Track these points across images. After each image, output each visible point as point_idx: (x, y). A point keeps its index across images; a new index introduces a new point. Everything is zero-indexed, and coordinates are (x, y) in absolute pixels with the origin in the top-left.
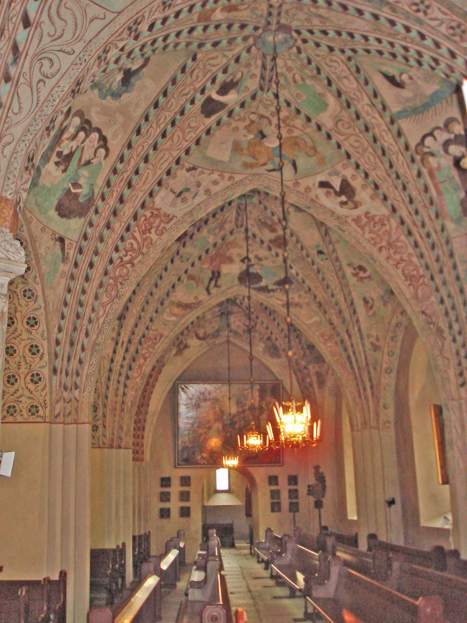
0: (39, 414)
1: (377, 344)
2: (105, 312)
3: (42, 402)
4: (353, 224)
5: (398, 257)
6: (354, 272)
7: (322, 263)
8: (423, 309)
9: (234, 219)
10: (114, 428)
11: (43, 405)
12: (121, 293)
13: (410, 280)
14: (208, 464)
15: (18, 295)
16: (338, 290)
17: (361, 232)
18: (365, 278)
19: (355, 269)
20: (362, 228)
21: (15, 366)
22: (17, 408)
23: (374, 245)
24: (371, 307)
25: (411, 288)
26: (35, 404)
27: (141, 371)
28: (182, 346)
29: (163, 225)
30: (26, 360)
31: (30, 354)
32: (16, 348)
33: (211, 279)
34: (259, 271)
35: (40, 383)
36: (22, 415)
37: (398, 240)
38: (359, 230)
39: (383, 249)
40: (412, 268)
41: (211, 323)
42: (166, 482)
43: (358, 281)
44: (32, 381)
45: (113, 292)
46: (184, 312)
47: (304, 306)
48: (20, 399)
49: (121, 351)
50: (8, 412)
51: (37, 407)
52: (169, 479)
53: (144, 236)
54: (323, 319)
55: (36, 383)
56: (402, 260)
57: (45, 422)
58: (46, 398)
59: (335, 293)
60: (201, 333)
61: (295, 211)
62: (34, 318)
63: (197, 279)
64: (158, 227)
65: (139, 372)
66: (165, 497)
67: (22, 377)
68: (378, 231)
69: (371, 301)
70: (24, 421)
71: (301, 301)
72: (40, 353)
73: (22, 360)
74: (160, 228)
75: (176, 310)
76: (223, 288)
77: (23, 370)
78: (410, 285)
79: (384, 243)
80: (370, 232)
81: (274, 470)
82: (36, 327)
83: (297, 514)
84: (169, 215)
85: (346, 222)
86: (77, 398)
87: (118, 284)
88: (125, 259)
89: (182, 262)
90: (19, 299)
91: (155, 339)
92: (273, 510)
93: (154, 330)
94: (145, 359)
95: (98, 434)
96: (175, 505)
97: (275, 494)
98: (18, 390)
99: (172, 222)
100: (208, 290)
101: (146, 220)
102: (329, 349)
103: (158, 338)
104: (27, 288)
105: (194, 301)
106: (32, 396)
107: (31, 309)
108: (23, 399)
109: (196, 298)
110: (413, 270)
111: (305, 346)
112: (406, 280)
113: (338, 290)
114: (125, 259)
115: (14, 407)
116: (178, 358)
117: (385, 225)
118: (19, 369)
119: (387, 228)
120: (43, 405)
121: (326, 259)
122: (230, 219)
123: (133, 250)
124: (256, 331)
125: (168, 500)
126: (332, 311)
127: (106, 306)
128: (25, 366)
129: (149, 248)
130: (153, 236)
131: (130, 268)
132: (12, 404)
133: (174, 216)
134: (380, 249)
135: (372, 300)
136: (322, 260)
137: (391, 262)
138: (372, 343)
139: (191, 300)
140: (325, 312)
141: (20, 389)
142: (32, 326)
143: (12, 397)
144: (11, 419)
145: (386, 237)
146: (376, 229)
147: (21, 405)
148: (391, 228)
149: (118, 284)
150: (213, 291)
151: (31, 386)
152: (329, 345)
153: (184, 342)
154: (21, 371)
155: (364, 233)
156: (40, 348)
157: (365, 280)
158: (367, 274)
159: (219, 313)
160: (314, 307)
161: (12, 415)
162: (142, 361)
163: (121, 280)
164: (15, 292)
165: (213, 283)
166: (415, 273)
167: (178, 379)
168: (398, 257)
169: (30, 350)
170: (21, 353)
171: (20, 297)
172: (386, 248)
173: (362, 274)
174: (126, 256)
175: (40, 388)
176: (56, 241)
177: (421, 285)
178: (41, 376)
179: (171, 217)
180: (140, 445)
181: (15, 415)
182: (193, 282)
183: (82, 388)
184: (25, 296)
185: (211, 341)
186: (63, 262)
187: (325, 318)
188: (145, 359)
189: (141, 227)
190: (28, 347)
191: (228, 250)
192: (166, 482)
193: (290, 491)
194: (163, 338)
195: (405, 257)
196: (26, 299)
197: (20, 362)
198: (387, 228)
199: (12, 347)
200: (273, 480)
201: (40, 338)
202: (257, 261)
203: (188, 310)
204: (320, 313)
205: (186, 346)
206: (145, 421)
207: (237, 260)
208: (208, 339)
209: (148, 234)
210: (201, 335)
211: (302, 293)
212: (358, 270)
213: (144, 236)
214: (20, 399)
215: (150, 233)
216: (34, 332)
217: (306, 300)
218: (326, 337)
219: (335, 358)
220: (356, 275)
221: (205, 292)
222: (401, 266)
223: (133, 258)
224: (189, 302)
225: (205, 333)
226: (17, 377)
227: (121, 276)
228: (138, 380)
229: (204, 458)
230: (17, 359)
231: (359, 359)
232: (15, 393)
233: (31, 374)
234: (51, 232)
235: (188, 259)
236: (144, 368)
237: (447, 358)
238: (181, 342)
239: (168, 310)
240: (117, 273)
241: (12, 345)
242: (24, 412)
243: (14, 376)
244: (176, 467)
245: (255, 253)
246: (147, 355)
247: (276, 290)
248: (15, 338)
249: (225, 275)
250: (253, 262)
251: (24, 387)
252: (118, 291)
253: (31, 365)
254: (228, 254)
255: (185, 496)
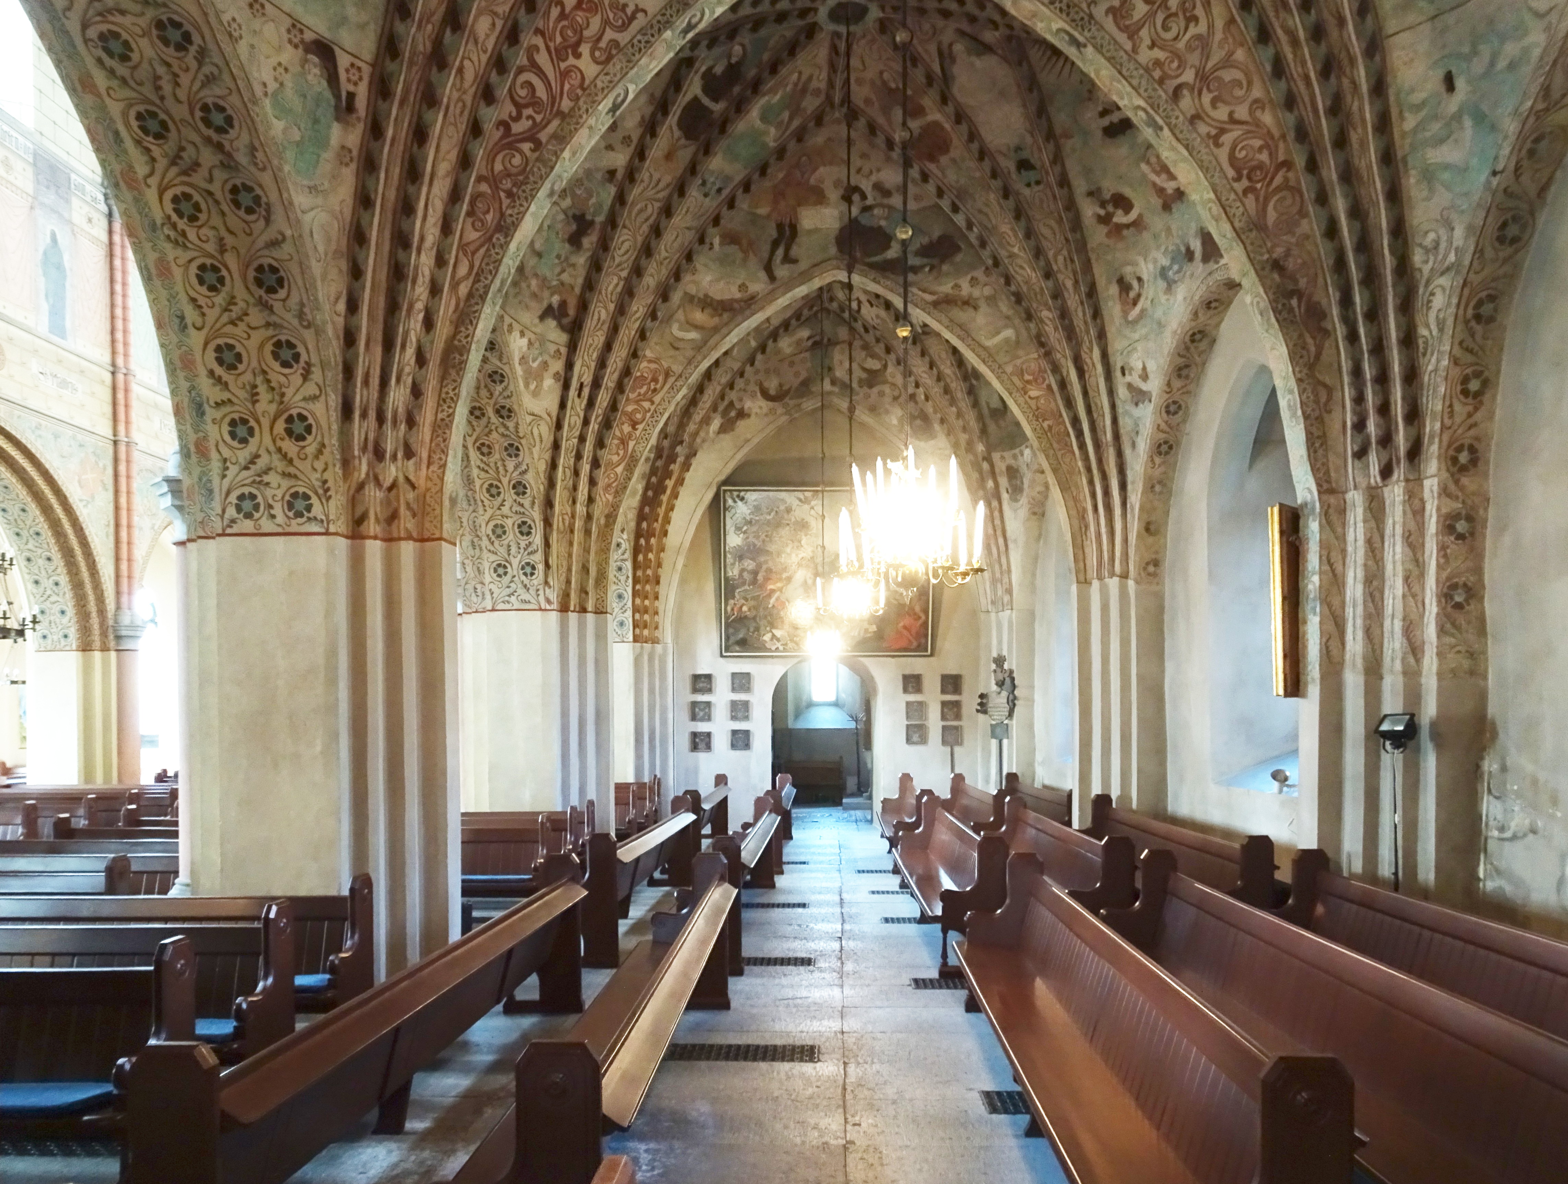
0: (311, 515)
1: (1144, 387)
2: (471, 267)
3: (317, 484)
4: (1109, 23)
5: (1221, 113)
6: (1102, 212)
7: (1027, 192)
8: (1275, 256)
9: (823, 85)
10: (569, 570)
11: (321, 491)
12: (509, 220)
13: (1249, 178)
14: (785, 650)
15: (217, 202)
16: (1060, 258)
17: (1128, 46)
18: (1128, 226)
19: (1103, 205)
20: (1132, 33)
21: (242, 394)
22: (260, 499)
23: (1161, 82)
24: (1135, 303)
25: (1250, 201)
26: (301, 490)
27: (626, 451)
28: (733, 414)
29: (609, 34)
30: (268, 381)
31: (276, 366)
32: (239, 348)
33: (775, 244)
34: (883, 223)
35: (310, 439)
36: (273, 517)
37: (1227, 63)
38: (1122, 38)
39: (1185, 92)
40: (1257, 143)
41: (792, 364)
42: (702, 682)
43: (1109, 235)
44: (289, 432)
45: (489, 217)
46: (716, 320)
47: (983, 305)
48: (266, 479)
49: (577, 406)
50: (239, 509)
51: (306, 497)
52: (709, 677)
53: (563, 65)
54: (1024, 333)
55: (300, 438)
56: (1233, 120)
57: (327, 533)
58: (326, 476)
59: (1055, 268)
60: (772, 385)
61: (969, 52)
62: (274, 270)
63: (744, 242)
64: (599, 39)
65: (621, 452)
66: (699, 712)
67: (265, 422)
68: (1176, 38)
69: (1135, 284)
70: (280, 530)
71: (976, 293)
72: (302, 364)
73: (259, 380)
74: (603, 44)
75: (699, 316)
76: (803, 265)
77: (266, 406)
78: (1245, 192)
79: (1188, 76)
80: (1153, 45)
81: (916, 665)
82: (282, 294)
83: (957, 749)
84: (625, 5)
85: (1091, 16)
86: (412, 477)
87: (502, 195)
88: (518, 128)
89: (706, 195)
90: (223, 214)
91: (655, 380)
92: (909, 741)
93: (650, 361)
94: (634, 425)
95: (535, 582)
96: (720, 727)
97: (915, 710)
98: (257, 456)
99: (635, 26)
100: (768, 269)
101: (563, 16)
102: (1033, 403)
103: (661, 379)
104: (238, 182)
105: (738, 295)
106: (292, 470)
107: (260, 243)
108: (272, 478)
109: (742, 287)
110: (1260, 149)
111: (986, 411)
112: (1238, 179)
113: (1060, 258)
114: (518, 128)
115: (253, 497)
116: (727, 438)
117: (1196, 19)
118: (254, 402)
119: (1202, 28)
120: (321, 491)
121: (1038, 183)
122: (815, 84)
123: (534, 102)
124: (885, 382)
125: (708, 718)
126: (1045, 314)
127: (474, 253)
128: (269, 396)
129: (578, 98)
130: (587, 65)
131: (528, 153)
132: (246, 490)
133: (638, 10)
134: (1176, 94)
135: (1140, 279)
136: (1028, 185)
137: (1203, 129)
138: (1130, 386)
139: (733, 293)
140: (1029, 317)
141: (262, 452)
142: (271, 290)
143: (245, 473)
144: (247, 525)
145: (1194, 59)
146: (1169, 36)
147: (269, 492)
148: (1211, 26)
149: (502, 195)
150: (782, 271)
151: (290, 447)
152: (1034, 393)
153: (738, 405)
154: (261, 407)
155: (1135, 50)
156: (301, 349)
157: (1125, 232)
158: (1133, 215)
159: (810, 343)
160: (1004, 307)
161: (249, 516)
162: (627, 428)
163: (507, 184)
164: (210, 193)
165: (780, 252)
166: (1264, 157)
167: (725, 482)
168: (1221, 113)
169: (276, 356)
170: (254, 364)
171: (225, 207)
172: (1192, 89)
173: (1120, 218)
174: (518, 118)
175: (311, 450)
176: (307, 50)
177: (1278, 189)
178: (311, 421)
179: (629, 10)
180: (651, 611)
181: (257, 515)
182: (732, 249)
183: (425, 455)
184: (237, 204)
185: (792, 403)
186: (338, 119)
187: (1028, 329)
188: (634, 425)
189: (552, 38)
190: (269, 347)
191: (815, 170)
192: (702, 682)
193: (944, 704)
194: (671, 380)
195: (1242, 113)
196: (242, 213)
197: (255, 386)
198: (1202, 28)
199: (231, 347)
200: (912, 683)
201: (295, 322)
202: (879, 200)
203: (726, 316)
204: (1017, 321)
205: (742, 414)
206: (659, 565)
207: (834, 195)
208: (787, 400)
209: (571, 61)
210: (772, 392)
211: (979, 274)
212: (1110, 208)
213: (563, 65)
214: (266, 479)
215: (578, 56)
216: (277, 306)
217: (988, 291)
218: (1027, 377)
219: (1045, 424)
220: (1105, 220)
221: (763, 275)
222: (1227, 139)
223: (537, 127)
224: (727, 296)
225: (781, 385)
226: (252, 423)
227: (509, 175)
228: (619, 470)
229: (778, 640)
230: (248, 377)
231: (1099, 424)
232: (252, 462)
233: (285, 416)
234: (288, 22)
235: (719, 191)
236: (631, 444)
237: (1325, 386)
238: (731, 404)
239: (680, 315)
240: (498, 167)
241: (231, 341)
242: (278, 510)
243: (244, 421)
244: (722, 656)
245: (874, 178)
246: (639, 416)
247: (922, 267)
248: (233, 323)
249: (810, 232)
250: (870, 201)
251: (272, 448)
252: (502, 215)
253: (283, 395)
254: (812, 181)
255: (740, 710)
